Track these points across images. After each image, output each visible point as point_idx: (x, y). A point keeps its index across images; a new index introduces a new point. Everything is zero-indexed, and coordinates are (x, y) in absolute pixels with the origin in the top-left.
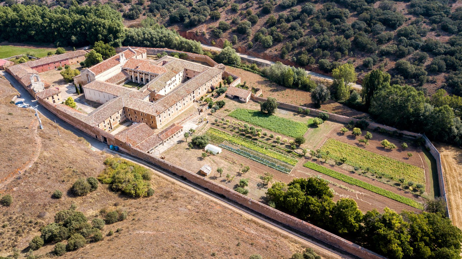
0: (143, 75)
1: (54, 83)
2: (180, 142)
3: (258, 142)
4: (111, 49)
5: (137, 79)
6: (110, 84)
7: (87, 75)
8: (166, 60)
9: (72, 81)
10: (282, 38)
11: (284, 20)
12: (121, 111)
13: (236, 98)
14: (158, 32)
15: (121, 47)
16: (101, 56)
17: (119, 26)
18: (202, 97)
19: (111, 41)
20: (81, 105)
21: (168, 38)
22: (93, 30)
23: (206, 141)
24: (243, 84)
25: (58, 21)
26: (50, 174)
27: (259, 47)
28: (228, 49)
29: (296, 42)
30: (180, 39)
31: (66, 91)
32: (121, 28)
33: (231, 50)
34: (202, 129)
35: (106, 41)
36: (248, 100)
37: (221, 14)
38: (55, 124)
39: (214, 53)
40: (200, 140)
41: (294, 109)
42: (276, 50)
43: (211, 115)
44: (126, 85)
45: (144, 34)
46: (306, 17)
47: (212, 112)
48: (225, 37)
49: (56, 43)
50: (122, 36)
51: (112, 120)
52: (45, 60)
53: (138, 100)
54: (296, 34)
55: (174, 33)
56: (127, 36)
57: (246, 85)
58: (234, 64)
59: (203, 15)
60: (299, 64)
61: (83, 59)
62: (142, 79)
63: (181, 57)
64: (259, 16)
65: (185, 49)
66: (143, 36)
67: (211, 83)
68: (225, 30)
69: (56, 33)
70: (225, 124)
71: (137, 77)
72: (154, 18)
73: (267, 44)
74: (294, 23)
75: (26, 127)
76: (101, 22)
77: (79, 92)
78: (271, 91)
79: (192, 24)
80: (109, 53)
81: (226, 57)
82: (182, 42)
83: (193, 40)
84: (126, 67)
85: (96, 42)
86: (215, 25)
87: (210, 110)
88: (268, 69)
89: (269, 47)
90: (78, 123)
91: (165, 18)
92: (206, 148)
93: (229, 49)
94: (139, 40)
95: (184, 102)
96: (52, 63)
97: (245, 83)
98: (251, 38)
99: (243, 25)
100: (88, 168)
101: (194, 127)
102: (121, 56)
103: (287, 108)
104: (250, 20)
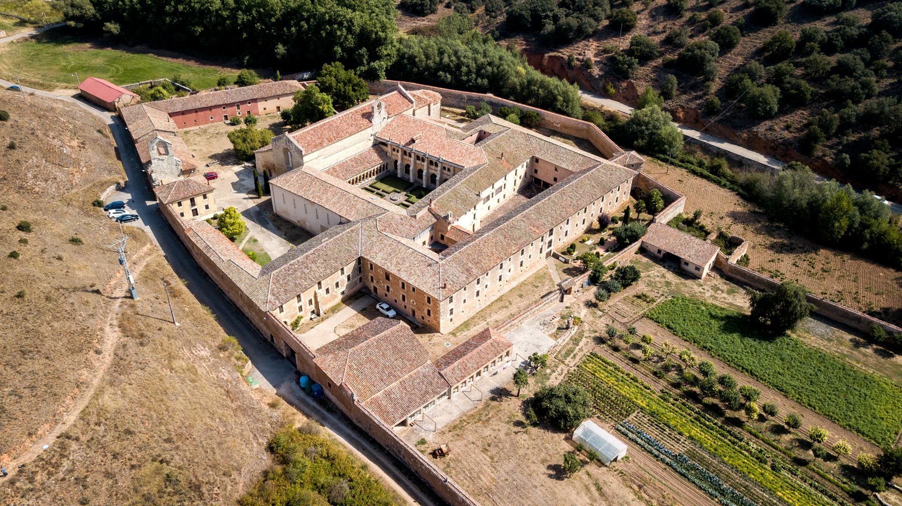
0: (425, 164)
1: (212, 157)
2: (500, 394)
3: (746, 436)
4: (358, 85)
5: (407, 171)
7: (286, 151)
8: (487, 128)
9: (251, 158)
10: (809, 96)
11: (816, 45)
12: (349, 269)
13: (671, 261)
14: (476, 51)
15: (384, 80)
16: (331, 101)
17: (384, 28)
18: (573, 247)
19: (362, 64)
20: (259, 228)
21: (498, 67)
22: (324, 34)
23: (580, 410)
24: (691, 216)
25: (254, 6)
26: (95, 482)
27: (736, 113)
28: (652, 112)
29: (854, 110)
30: (527, 73)
31: (233, 184)
32: (390, 35)
33: (661, 115)
34: (567, 354)
35: (350, 62)
36: (706, 270)
37: (639, 16)
38: (179, 284)
39: (611, 118)
40: (561, 403)
41: (853, 324)
42: (788, 128)
43: (595, 305)
45: (441, 53)
46: (887, 41)
47: (599, 297)
48: (642, 79)
49: (243, 59)
50: (388, 55)
51: (321, 293)
52: (206, 96)
53: (398, 240)
54: (854, 88)
55: (515, 56)
56: (401, 56)
57: (703, 221)
58: (664, 152)
59: (591, 16)
60: (860, 175)
61: (288, 103)
62: (421, 171)
63: (526, 121)
64: (741, 31)
65: (537, 99)
67: (602, 205)
68: (644, 58)
69: (245, 35)
70: (637, 346)
71: (408, 166)
72: (470, 16)
73: (765, 109)
74: (848, 57)
75: (95, 288)
76: (345, 17)
77: (261, 192)
78: (772, 247)
79: (563, 37)
80: (351, 93)
82: (531, 82)
83: (560, 79)
84: (386, 137)
85: (326, 65)
86: (623, 43)
87: (594, 289)
88: (765, 183)
89: (769, 116)
91: (495, 17)
92: (578, 433)
93: (655, 111)
94: (427, 68)
96: (219, 106)
97: (697, 215)
98: (715, 86)
99: (697, 51)
100: (214, 467)
103: (832, 316)
104: (715, 38)
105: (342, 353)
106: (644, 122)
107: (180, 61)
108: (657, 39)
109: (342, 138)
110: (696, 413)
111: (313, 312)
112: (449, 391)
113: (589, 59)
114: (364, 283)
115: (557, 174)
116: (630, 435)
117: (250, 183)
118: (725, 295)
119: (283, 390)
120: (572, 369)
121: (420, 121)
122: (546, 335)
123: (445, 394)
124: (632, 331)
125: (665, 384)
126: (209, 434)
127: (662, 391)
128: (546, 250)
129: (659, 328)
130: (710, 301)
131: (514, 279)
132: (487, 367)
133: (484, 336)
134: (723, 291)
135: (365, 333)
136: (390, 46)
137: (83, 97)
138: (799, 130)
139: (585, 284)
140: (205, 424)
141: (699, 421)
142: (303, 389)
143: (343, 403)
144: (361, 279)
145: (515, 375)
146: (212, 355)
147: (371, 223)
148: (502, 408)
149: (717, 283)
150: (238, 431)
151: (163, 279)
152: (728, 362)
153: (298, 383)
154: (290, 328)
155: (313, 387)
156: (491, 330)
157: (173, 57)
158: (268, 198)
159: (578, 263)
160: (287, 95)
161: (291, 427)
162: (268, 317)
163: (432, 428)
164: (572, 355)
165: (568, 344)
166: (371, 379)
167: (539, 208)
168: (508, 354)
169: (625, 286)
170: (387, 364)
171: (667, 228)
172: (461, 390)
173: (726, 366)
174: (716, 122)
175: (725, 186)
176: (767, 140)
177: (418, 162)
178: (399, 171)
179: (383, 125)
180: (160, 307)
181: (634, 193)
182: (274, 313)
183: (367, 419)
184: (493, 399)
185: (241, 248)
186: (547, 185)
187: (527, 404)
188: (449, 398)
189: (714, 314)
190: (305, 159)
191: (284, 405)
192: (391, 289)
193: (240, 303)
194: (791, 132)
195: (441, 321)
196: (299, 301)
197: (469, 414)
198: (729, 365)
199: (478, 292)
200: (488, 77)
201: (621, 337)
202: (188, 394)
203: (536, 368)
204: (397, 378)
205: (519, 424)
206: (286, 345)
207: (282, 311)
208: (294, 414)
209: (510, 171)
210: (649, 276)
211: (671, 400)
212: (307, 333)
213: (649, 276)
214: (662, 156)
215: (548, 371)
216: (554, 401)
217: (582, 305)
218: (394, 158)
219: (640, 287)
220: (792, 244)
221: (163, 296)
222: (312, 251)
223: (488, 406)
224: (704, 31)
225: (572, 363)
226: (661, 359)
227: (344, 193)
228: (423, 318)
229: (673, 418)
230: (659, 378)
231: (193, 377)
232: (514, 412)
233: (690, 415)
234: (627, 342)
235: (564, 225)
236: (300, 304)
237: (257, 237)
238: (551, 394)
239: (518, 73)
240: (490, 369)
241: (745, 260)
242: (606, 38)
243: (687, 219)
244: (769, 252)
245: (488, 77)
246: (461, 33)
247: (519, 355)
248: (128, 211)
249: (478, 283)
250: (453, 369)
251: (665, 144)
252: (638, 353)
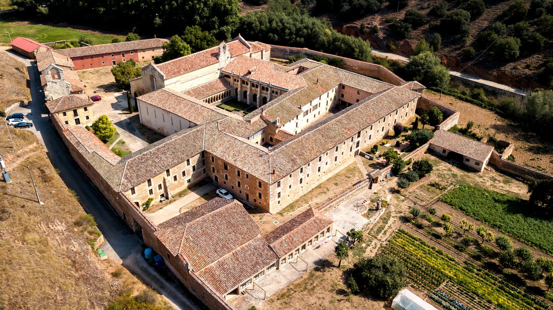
0: (259, 89)
1: (98, 87)
2: (323, 265)
5: (245, 97)
6: (193, 99)
7: (152, 77)
8: (304, 65)
10: (542, 44)
12: (194, 161)
13: (455, 159)
18: (375, 147)
20: (127, 134)
21: (312, 30)
23: (398, 280)
24: (464, 127)
27: (488, 58)
28: (426, 56)
30: (333, 34)
34: (379, 231)
35: (206, 27)
38: (52, 172)
40: (380, 273)
42: (528, 67)
43: (398, 192)
44: (223, 106)
45: (271, 21)
50: (233, 22)
51: (170, 180)
53: (238, 143)
57: (475, 130)
58: (436, 85)
62: (255, 96)
63: (331, 62)
66: (268, 25)
67: (396, 117)
70: (438, 225)
71: (245, 92)
73: (510, 54)
78: (530, 150)
81: (419, 71)
82: (335, 39)
85: (188, 27)
86: (401, 15)
87: (396, 179)
89: (513, 59)
93: (429, 57)
94: (261, 31)
95: (336, 154)
96: (109, 54)
97: (470, 125)
98: (469, 41)
101: (360, 223)
102: (222, 49)
105: (180, 227)
106: (421, 64)
107: (89, 31)
108: (424, 13)
110: (499, 282)
111: (162, 196)
112: (278, 262)
113: (376, 26)
114: (208, 174)
115: (358, 97)
116: (444, 303)
117: (125, 104)
118: (502, 184)
119: (129, 261)
120: (384, 243)
121: (255, 59)
122: (360, 215)
123: (273, 265)
124: (432, 212)
125: (467, 256)
126: (45, 303)
127: (465, 263)
128: (355, 150)
129: (453, 210)
130: (491, 189)
131: (330, 171)
132: (311, 241)
133: (308, 214)
134: (500, 181)
135: (203, 210)
136: (234, 16)
137: (15, 51)
138: (537, 68)
139: (388, 175)
140: (44, 293)
141: (504, 290)
142: (147, 260)
143: (180, 273)
144: (204, 170)
145: (337, 249)
146: (68, 229)
147: (213, 125)
148: (325, 278)
149: (494, 175)
150: (75, 299)
151: (39, 168)
152: (517, 237)
153: (143, 255)
154: (141, 209)
155: (155, 258)
156: (313, 209)
157: (84, 30)
158: (136, 113)
159: (382, 160)
160: (159, 48)
161: (129, 296)
162: (120, 198)
163: (262, 296)
164: (383, 232)
165: (378, 222)
166: (206, 250)
167: (348, 116)
168: (328, 230)
169: (421, 176)
170: (221, 237)
171: (449, 133)
172: (288, 261)
173: (516, 241)
174: (472, 65)
175: (485, 107)
176: (513, 75)
177: (253, 88)
178: (239, 96)
179: (228, 62)
180: (29, 189)
181: (418, 111)
182: (125, 194)
183: (200, 287)
184: (317, 269)
185: (111, 148)
186: (350, 105)
187: (348, 274)
188: (277, 269)
189: (497, 198)
190: (166, 82)
191: (127, 274)
192: (229, 177)
193: (102, 188)
194: (530, 70)
195: (271, 203)
196: (150, 185)
197: (296, 283)
198: (519, 241)
199: (301, 180)
200: (304, 37)
201: (424, 217)
202: (33, 264)
203: (353, 242)
204: (229, 249)
205: (341, 292)
206: (135, 221)
207: (133, 192)
208: (133, 283)
209: (324, 93)
210: (438, 170)
211: (475, 270)
212: (157, 213)
213: (438, 170)
214: (434, 88)
215: (364, 245)
216: (373, 271)
217: (387, 191)
218: (235, 86)
219: (432, 177)
220: (546, 147)
221: (38, 180)
222: (163, 145)
223: (313, 276)
225: (383, 238)
226: (459, 235)
227: (193, 104)
228: (255, 200)
229: (480, 287)
230: (461, 251)
231: (43, 248)
232: (336, 281)
233: (494, 284)
234: (429, 220)
235: (368, 129)
236: (150, 188)
237: (124, 140)
238: (370, 264)
239: (325, 34)
240: (314, 243)
241: (511, 157)
242: (387, 13)
243: (461, 129)
244: (529, 153)
245: (304, 37)
246: (284, 9)
247: (339, 231)
248: (25, 121)
249: (301, 171)
250: (281, 243)
251: (437, 79)
252: (440, 230)
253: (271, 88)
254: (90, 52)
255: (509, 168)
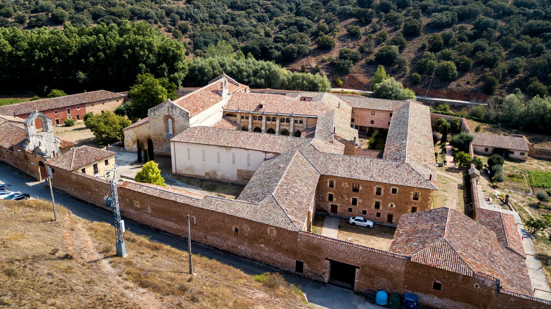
15: (181, 88)
22: (127, 56)
42: (468, 83)
49: (43, 88)
50: (183, 68)
75: (61, 253)
89: (453, 79)
90: (214, 229)
103: (230, 243)
109: (209, 106)
177: (268, 122)
224: (379, 44)
253: (294, 117)
254: (26, 110)
255: (542, 154)
